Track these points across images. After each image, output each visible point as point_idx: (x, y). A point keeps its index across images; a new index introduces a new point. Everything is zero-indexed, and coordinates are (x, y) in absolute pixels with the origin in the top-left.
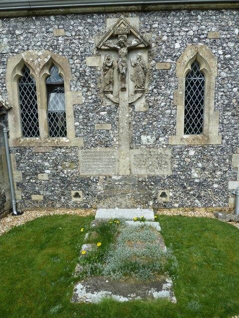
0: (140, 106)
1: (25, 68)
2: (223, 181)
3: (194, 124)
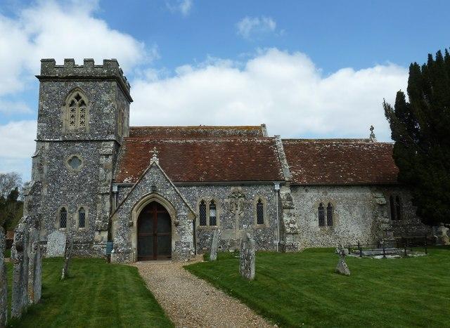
0: (242, 215)
1: (203, 202)
2: (272, 240)
3: (260, 221)
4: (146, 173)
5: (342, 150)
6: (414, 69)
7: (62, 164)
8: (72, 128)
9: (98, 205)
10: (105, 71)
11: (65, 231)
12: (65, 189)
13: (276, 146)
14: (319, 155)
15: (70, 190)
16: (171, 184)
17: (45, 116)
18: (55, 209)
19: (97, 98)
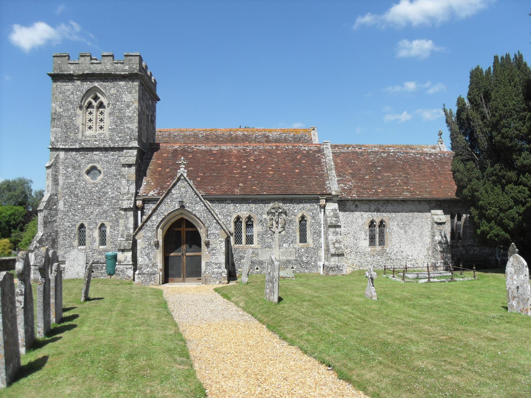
1: (238, 218)
2: (315, 261)
3: (303, 239)
4: (173, 187)
5: (401, 160)
6: (476, 76)
7: (79, 175)
8: (88, 133)
9: (120, 221)
10: (127, 67)
11: (85, 250)
12: (84, 202)
13: (324, 155)
14: (374, 166)
15: (89, 204)
16: (200, 199)
17: (59, 119)
18: (73, 225)
19: (118, 98)
